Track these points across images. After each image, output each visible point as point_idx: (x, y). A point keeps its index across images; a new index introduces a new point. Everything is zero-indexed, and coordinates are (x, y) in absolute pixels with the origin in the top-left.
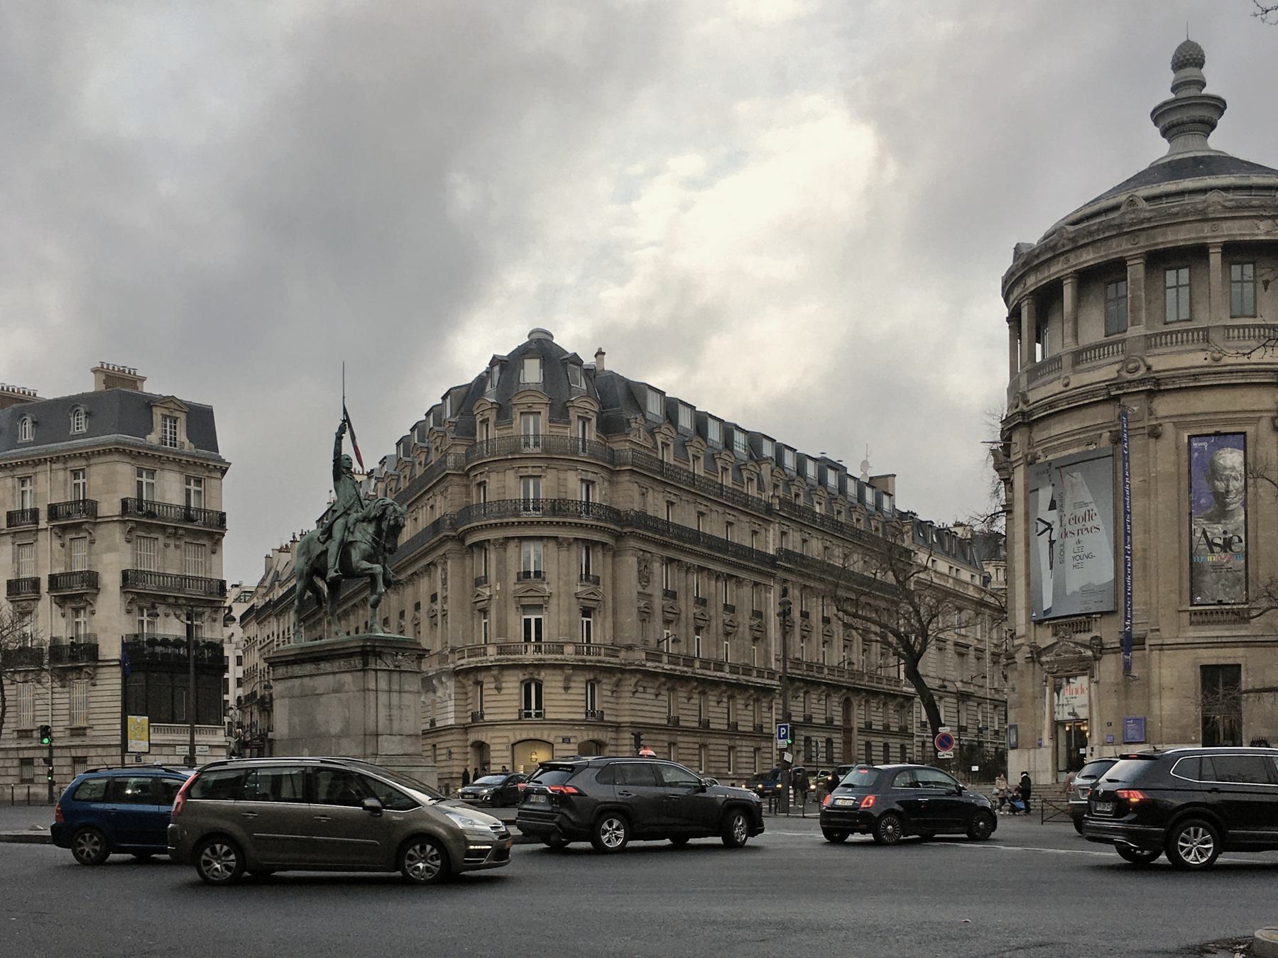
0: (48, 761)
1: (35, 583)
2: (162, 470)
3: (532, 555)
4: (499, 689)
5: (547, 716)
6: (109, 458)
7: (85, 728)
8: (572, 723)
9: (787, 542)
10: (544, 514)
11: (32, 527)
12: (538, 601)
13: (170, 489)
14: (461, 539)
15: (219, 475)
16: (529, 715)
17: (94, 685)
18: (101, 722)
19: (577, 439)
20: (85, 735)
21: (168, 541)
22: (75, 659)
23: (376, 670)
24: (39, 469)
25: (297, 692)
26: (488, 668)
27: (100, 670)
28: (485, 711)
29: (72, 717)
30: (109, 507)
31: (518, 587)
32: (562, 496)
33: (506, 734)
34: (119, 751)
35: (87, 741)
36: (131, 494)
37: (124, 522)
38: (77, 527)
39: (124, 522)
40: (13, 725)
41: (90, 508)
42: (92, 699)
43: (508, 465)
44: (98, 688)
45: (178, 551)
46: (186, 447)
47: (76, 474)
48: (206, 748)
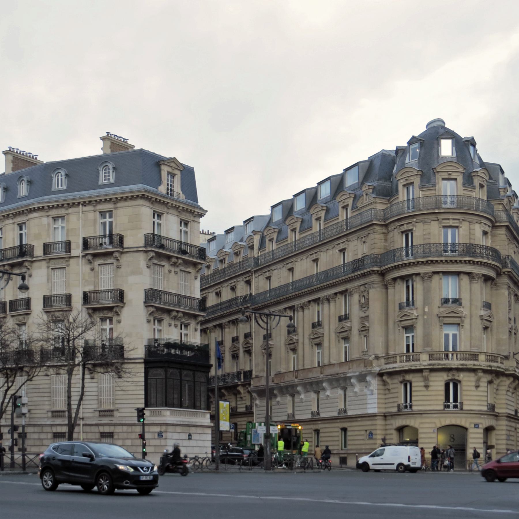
2: (168, 213)
3: (449, 288)
4: (427, 386)
5: (465, 407)
7: (112, 411)
8: (480, 413)
10: (460, 255)
11: (64, 255)
12: (457, 321)
14: (382, 274)
16: (448, 406)
17: (120, 377)
18: (125, 406)
20: (112, 416)
22: (107, 358)
23: (173, 379)
24: (70, 210)
26: (420, 371)
27: (125, 366)
28: (238, 406)
29: (100, 402)
30: (134, 239)
31: (442, 309)
32: (472, 242)
33: (434, 420)
36: (150, 231)
37: (146, 252)
38: (109, 254)
39: (146, 252)
40: (48, 407)
43: (434, 217)
45: (176, 276)
47: (102, 214)
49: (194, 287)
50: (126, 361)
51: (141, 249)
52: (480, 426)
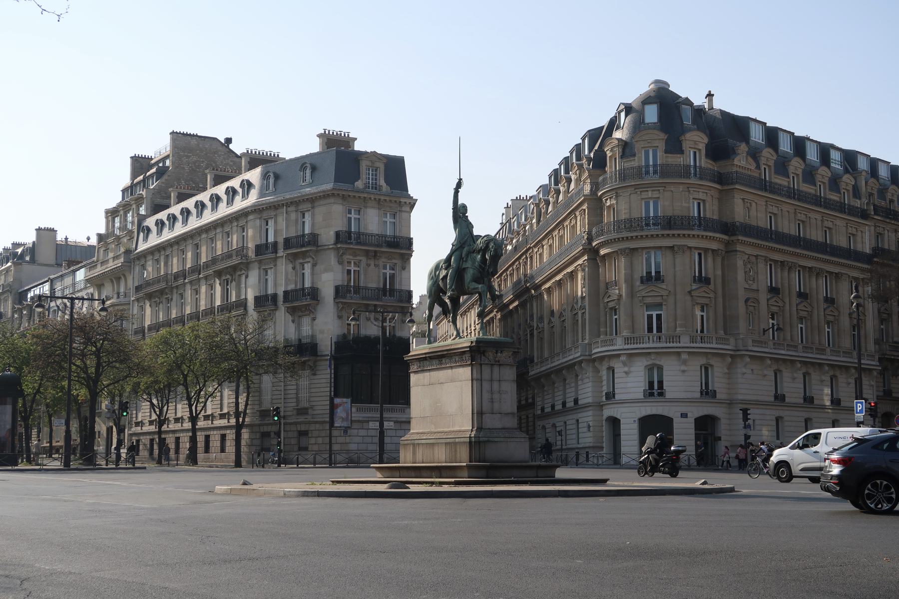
0: (278, 434)
2: (366, 207)
8: (691, 401)
9: (883, 240)
12: (658, 300)
13: (373, 222)
15: (408, 209)
16: (652, 394)
17: (314, 374)
19: (689, 166)
20: (307, 413)
21: (369, 262)
24: (279, 211)
25: (426, 382)
29: (298, 400)
30: (327, 237)
35: (309, 418)
39: (338, 249)
41: (314, 239)
42: (313, 386)
44: (317, 377)
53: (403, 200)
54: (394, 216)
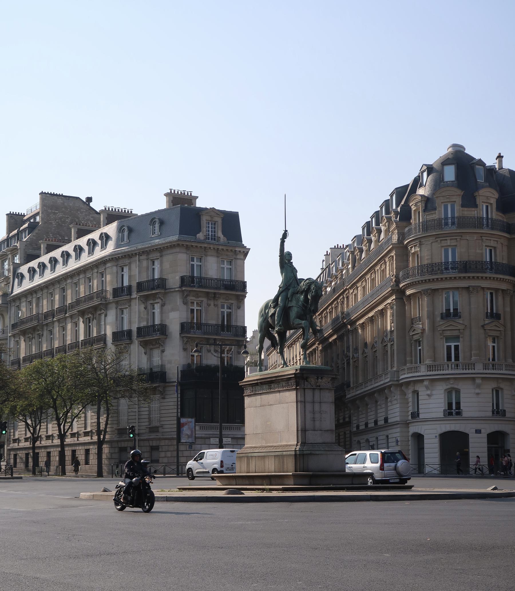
1: (130, 332)
6: (174, 250)
12: (456, 333)
13: (213, 268)
15: (242, 257)
16: (450, 414)
19: (483, 218)
21: (209, 302)
24: (132, 260)
30: (174, 281)
34: (175, 442)
35: (160, 435)
39: (183, 291)
41: (162, 283)
42: (162, 408)
44: (165, 400)
46: (222, 240)
48: (230, 439)
49: (237, 316)
50: (167, 384)
51: (177, 289)
52: (483, 431)
53: (238, 249)
54: (230, 263)
